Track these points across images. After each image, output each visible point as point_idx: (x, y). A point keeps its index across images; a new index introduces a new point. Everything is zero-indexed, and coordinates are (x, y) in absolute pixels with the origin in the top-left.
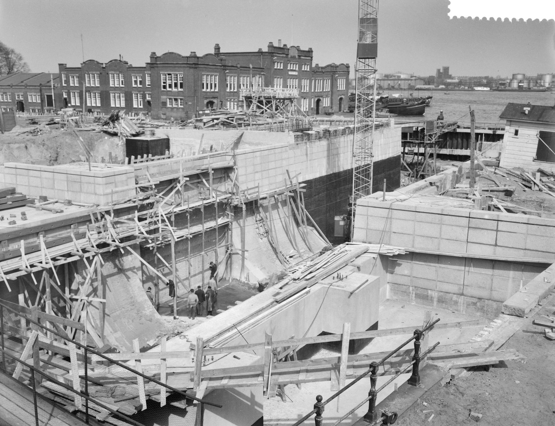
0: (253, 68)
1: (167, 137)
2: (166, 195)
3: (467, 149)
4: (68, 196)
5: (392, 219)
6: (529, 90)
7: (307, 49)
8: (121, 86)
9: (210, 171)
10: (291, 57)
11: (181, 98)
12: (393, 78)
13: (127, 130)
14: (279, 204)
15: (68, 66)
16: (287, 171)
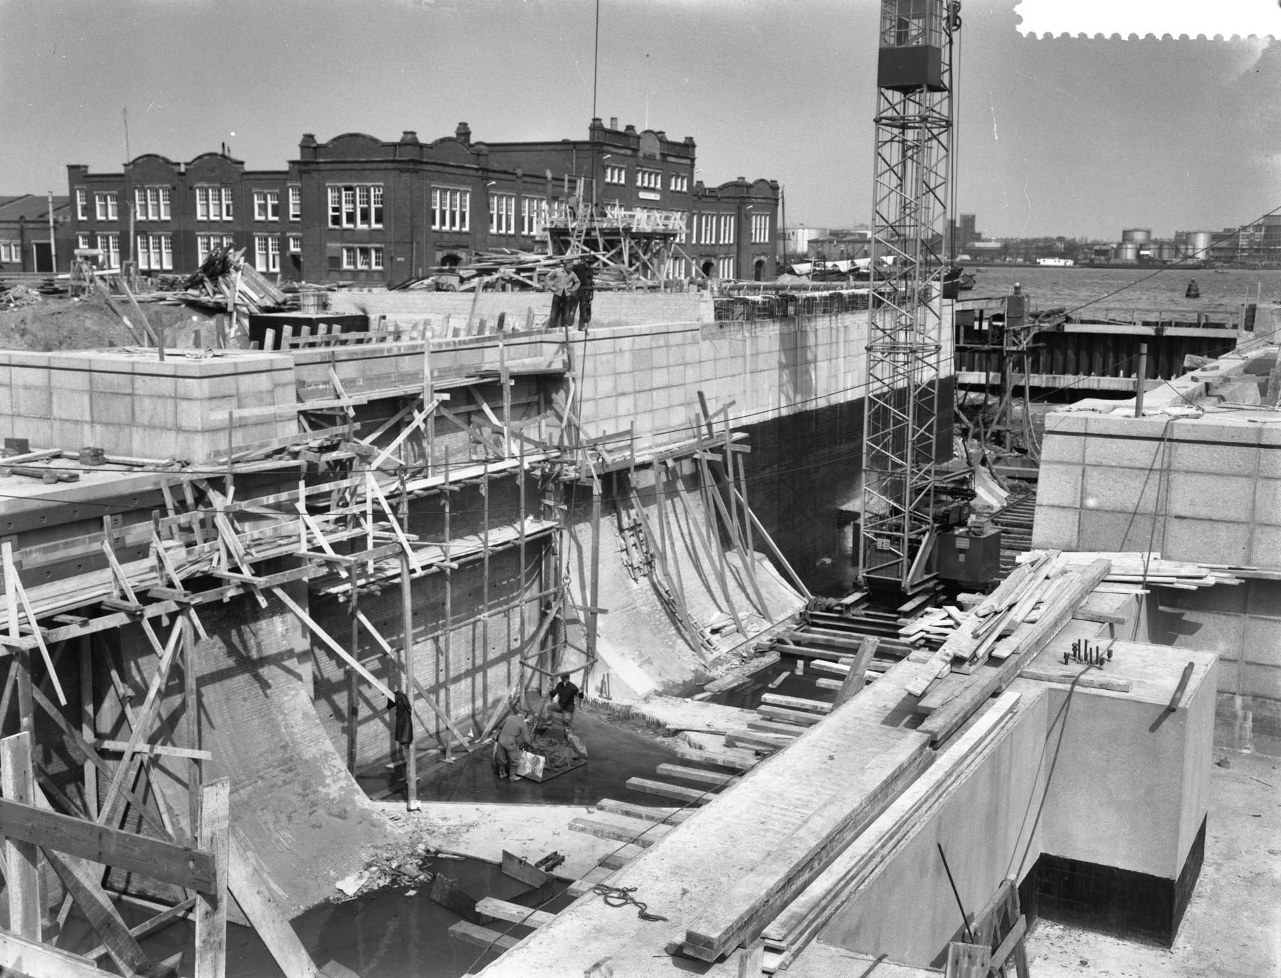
0: (554, 179)
1: (361, 313)
2: (382, 442)
3: (1089, 374)
4: (91, 438)
5: (1173, 476)
6: (1164, 265)
7: (682, 140)
8: (225, 218)
9: (503, 380)
10: (645, 157)
11: (378, 245)
12: (848, 238)
13: (250, 299)
14: (680, 486)
15: (91, 171)
16: (701, 394)
